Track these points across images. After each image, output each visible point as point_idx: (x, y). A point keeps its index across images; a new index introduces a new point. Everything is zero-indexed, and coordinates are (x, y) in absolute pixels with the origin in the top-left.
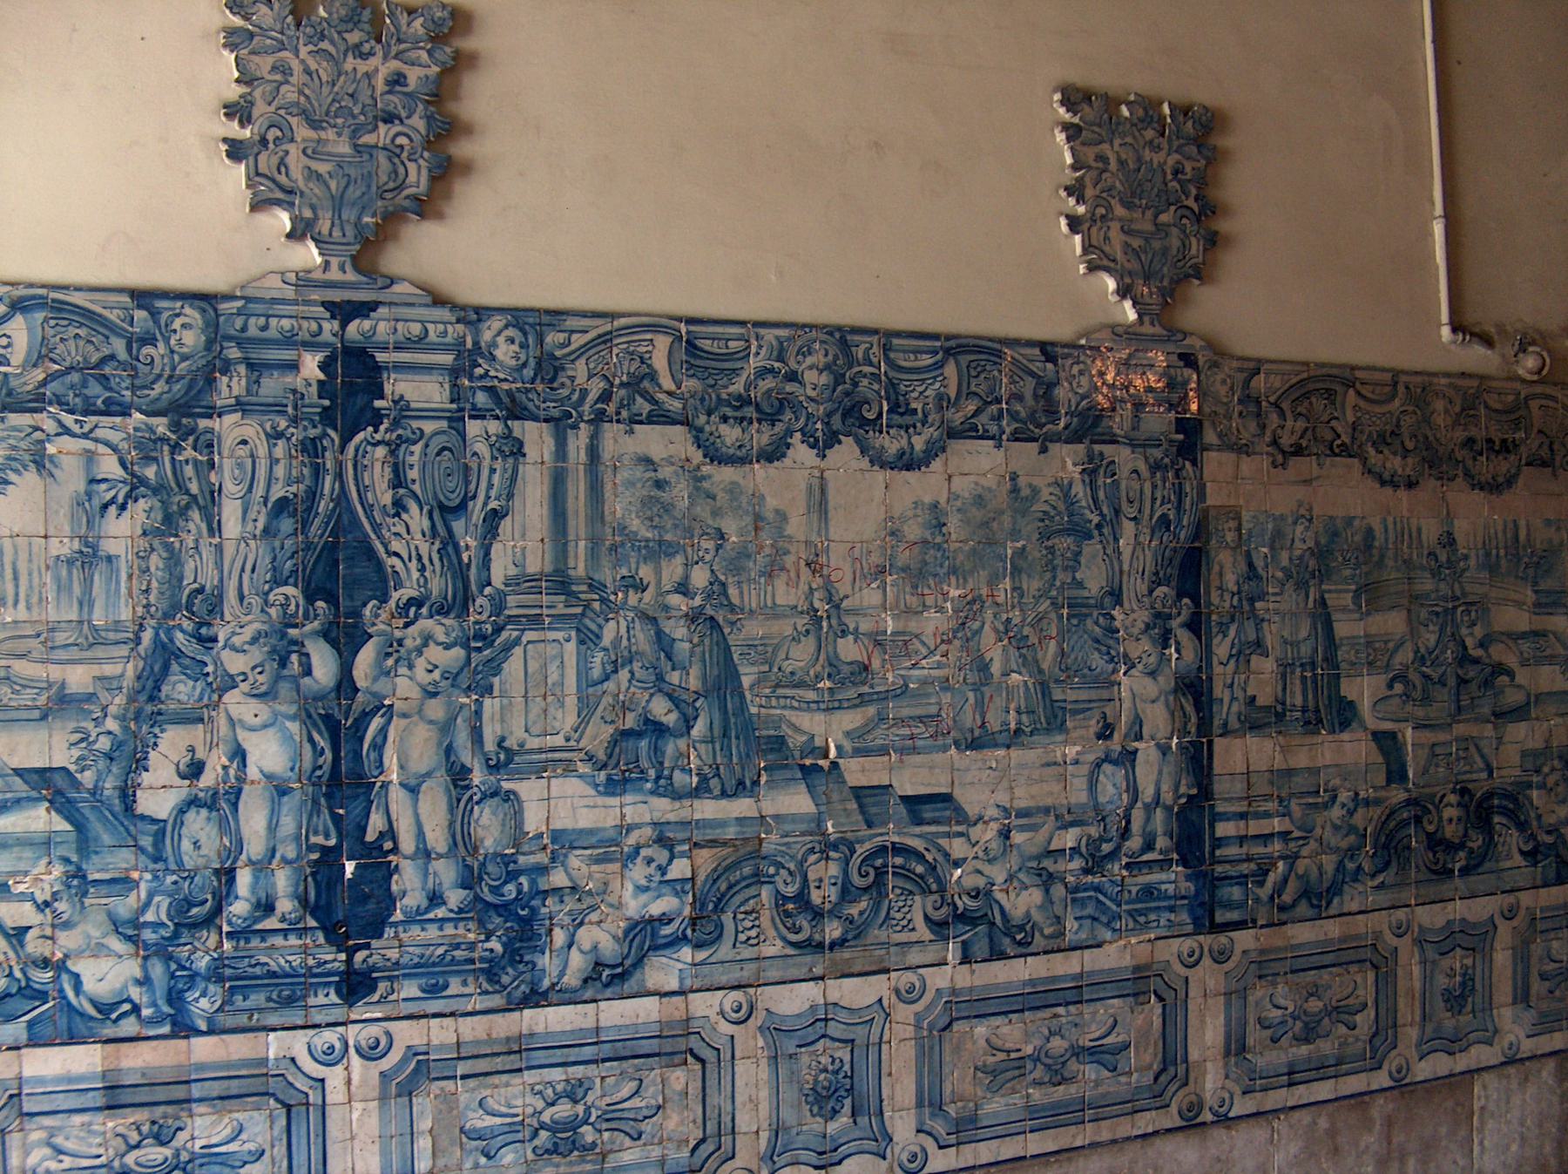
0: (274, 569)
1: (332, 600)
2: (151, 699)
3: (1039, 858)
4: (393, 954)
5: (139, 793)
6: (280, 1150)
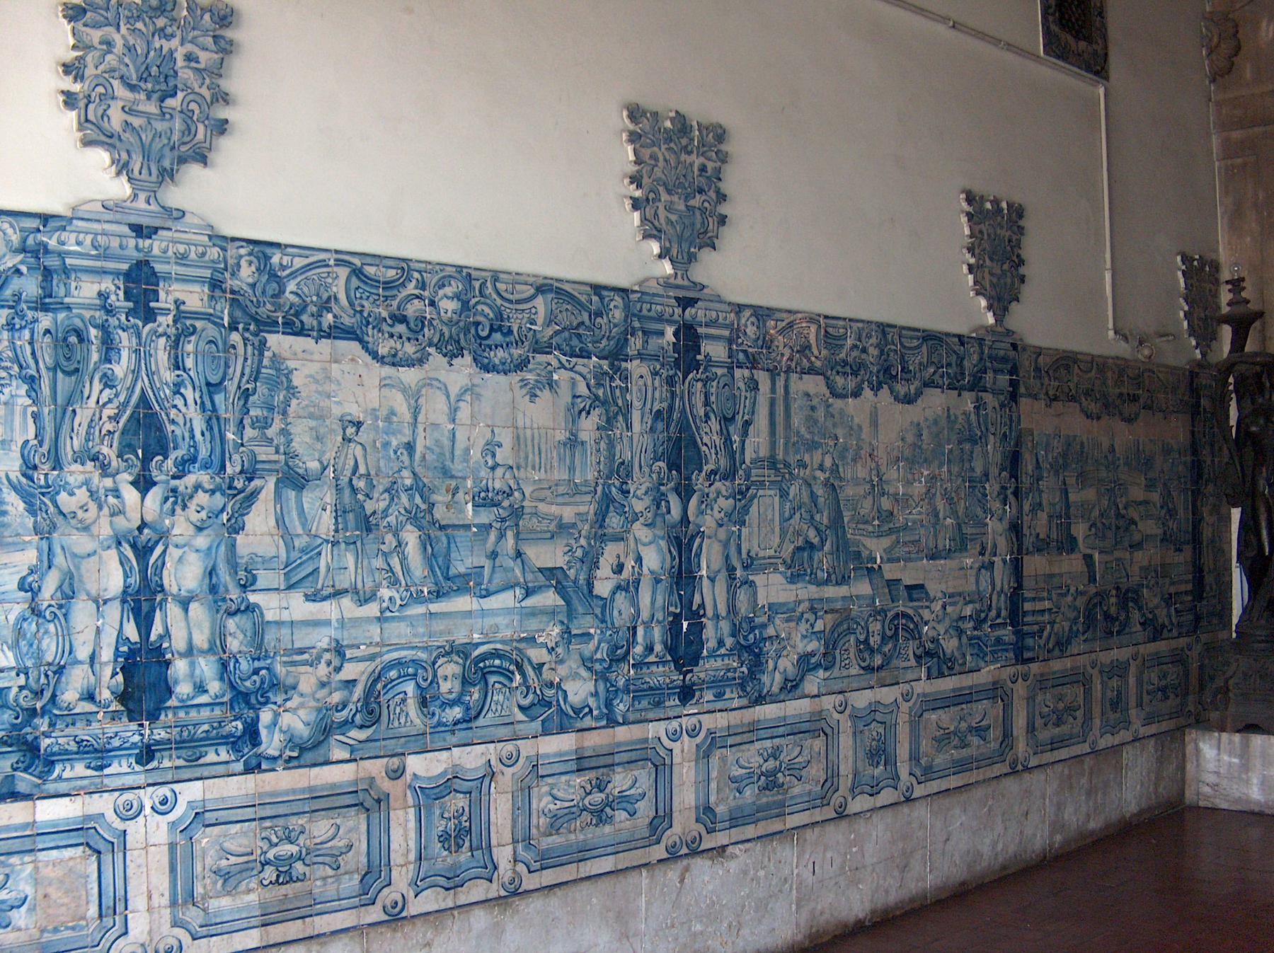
1: (679, 471)
2: (601, 526)
3: (957, 621)
4: (702, 675)
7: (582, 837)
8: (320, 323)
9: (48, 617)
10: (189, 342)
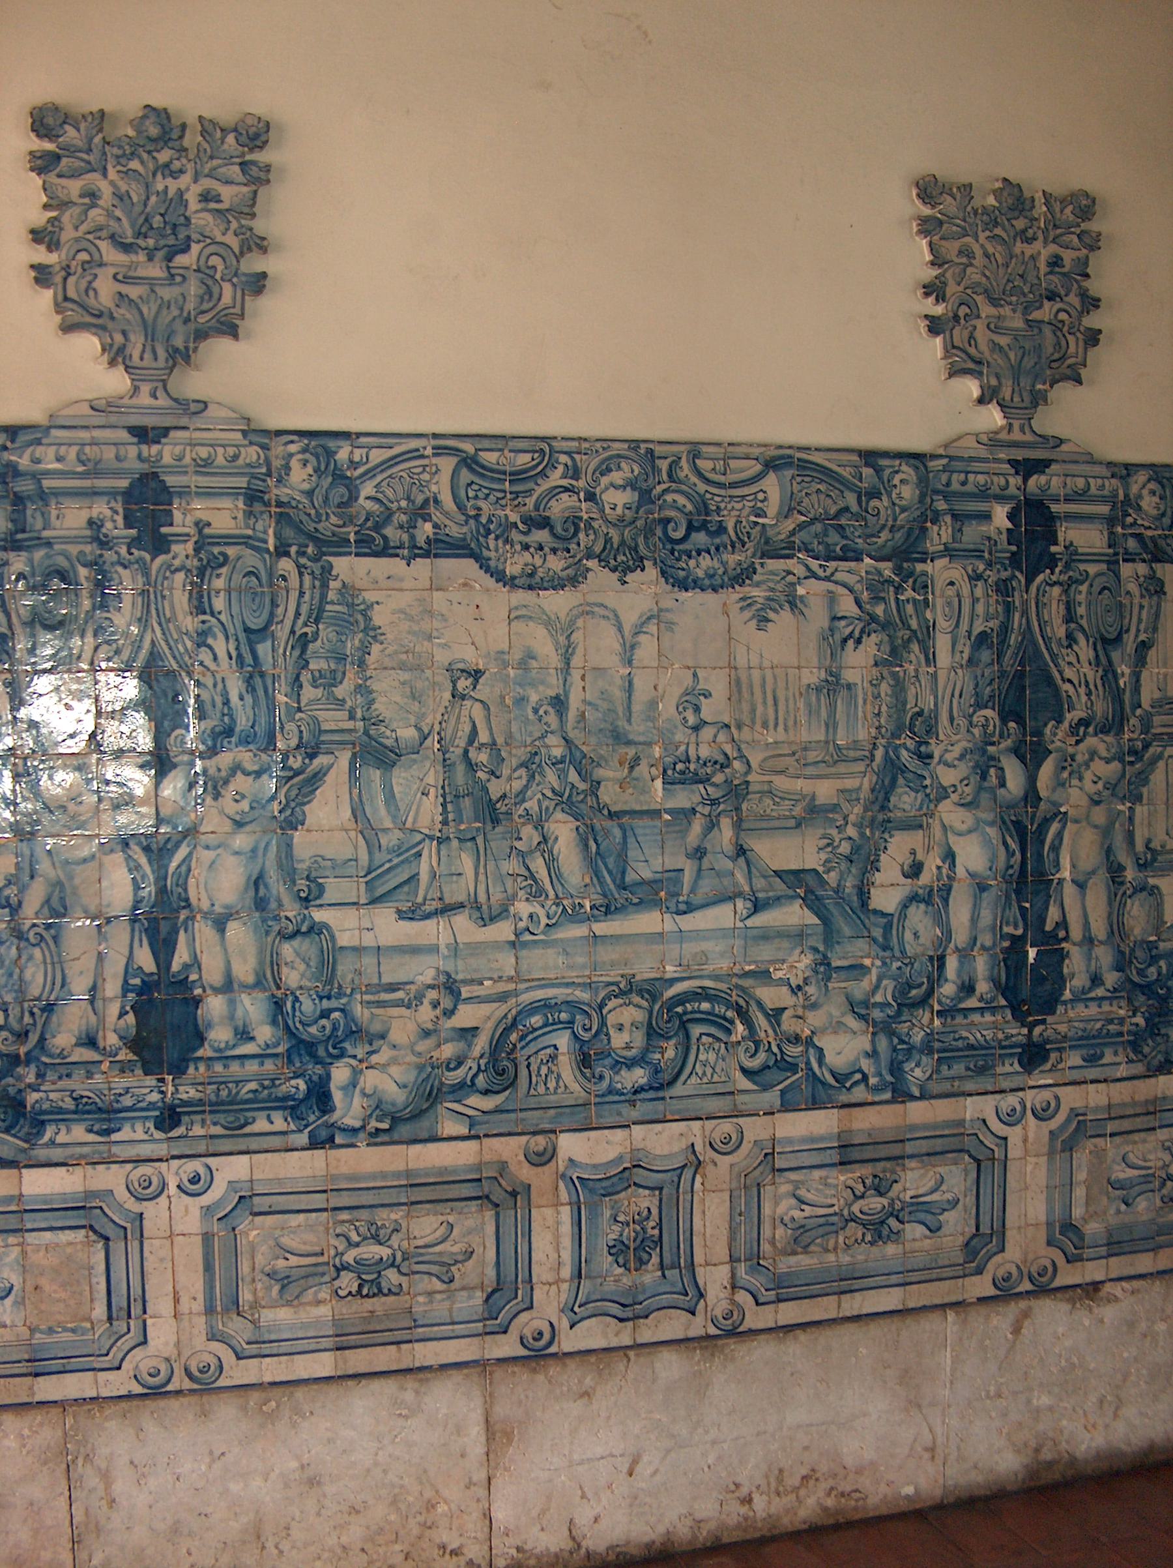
0: (977, 694)
1: (1020, 721)
4: (1063, 1028)
5: (872, 891)
6: (970, 1200)
7: (846, 1259)
8: (412, 537)
9: (32, 940)
10: (218, 576)
